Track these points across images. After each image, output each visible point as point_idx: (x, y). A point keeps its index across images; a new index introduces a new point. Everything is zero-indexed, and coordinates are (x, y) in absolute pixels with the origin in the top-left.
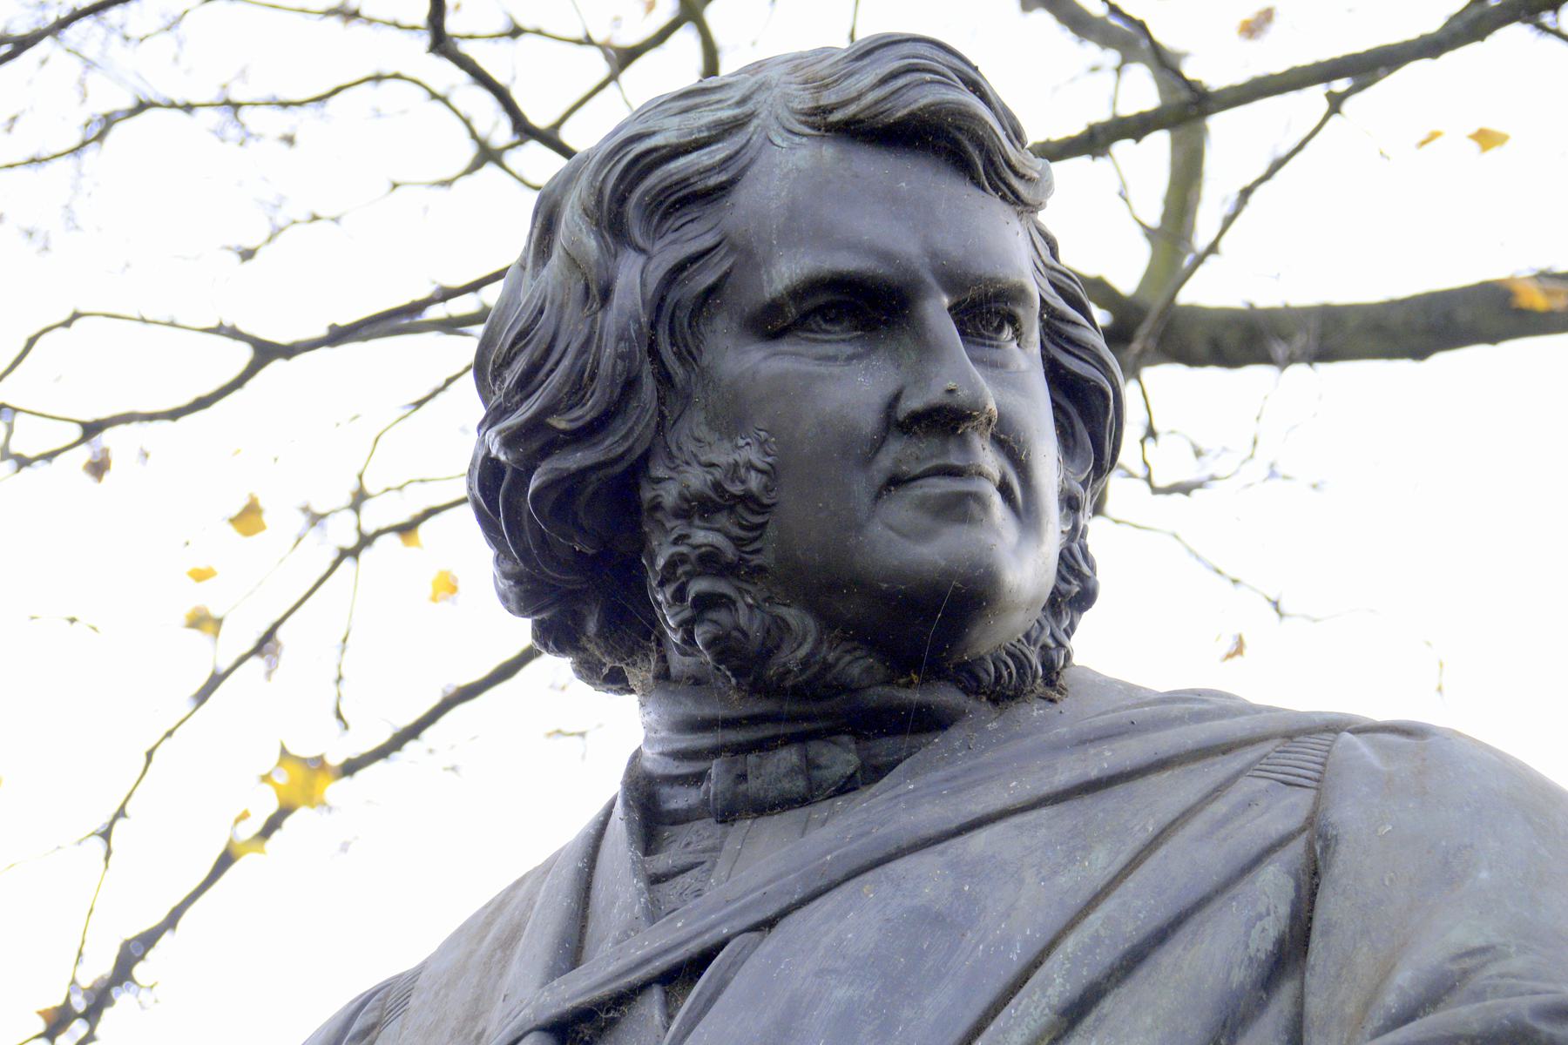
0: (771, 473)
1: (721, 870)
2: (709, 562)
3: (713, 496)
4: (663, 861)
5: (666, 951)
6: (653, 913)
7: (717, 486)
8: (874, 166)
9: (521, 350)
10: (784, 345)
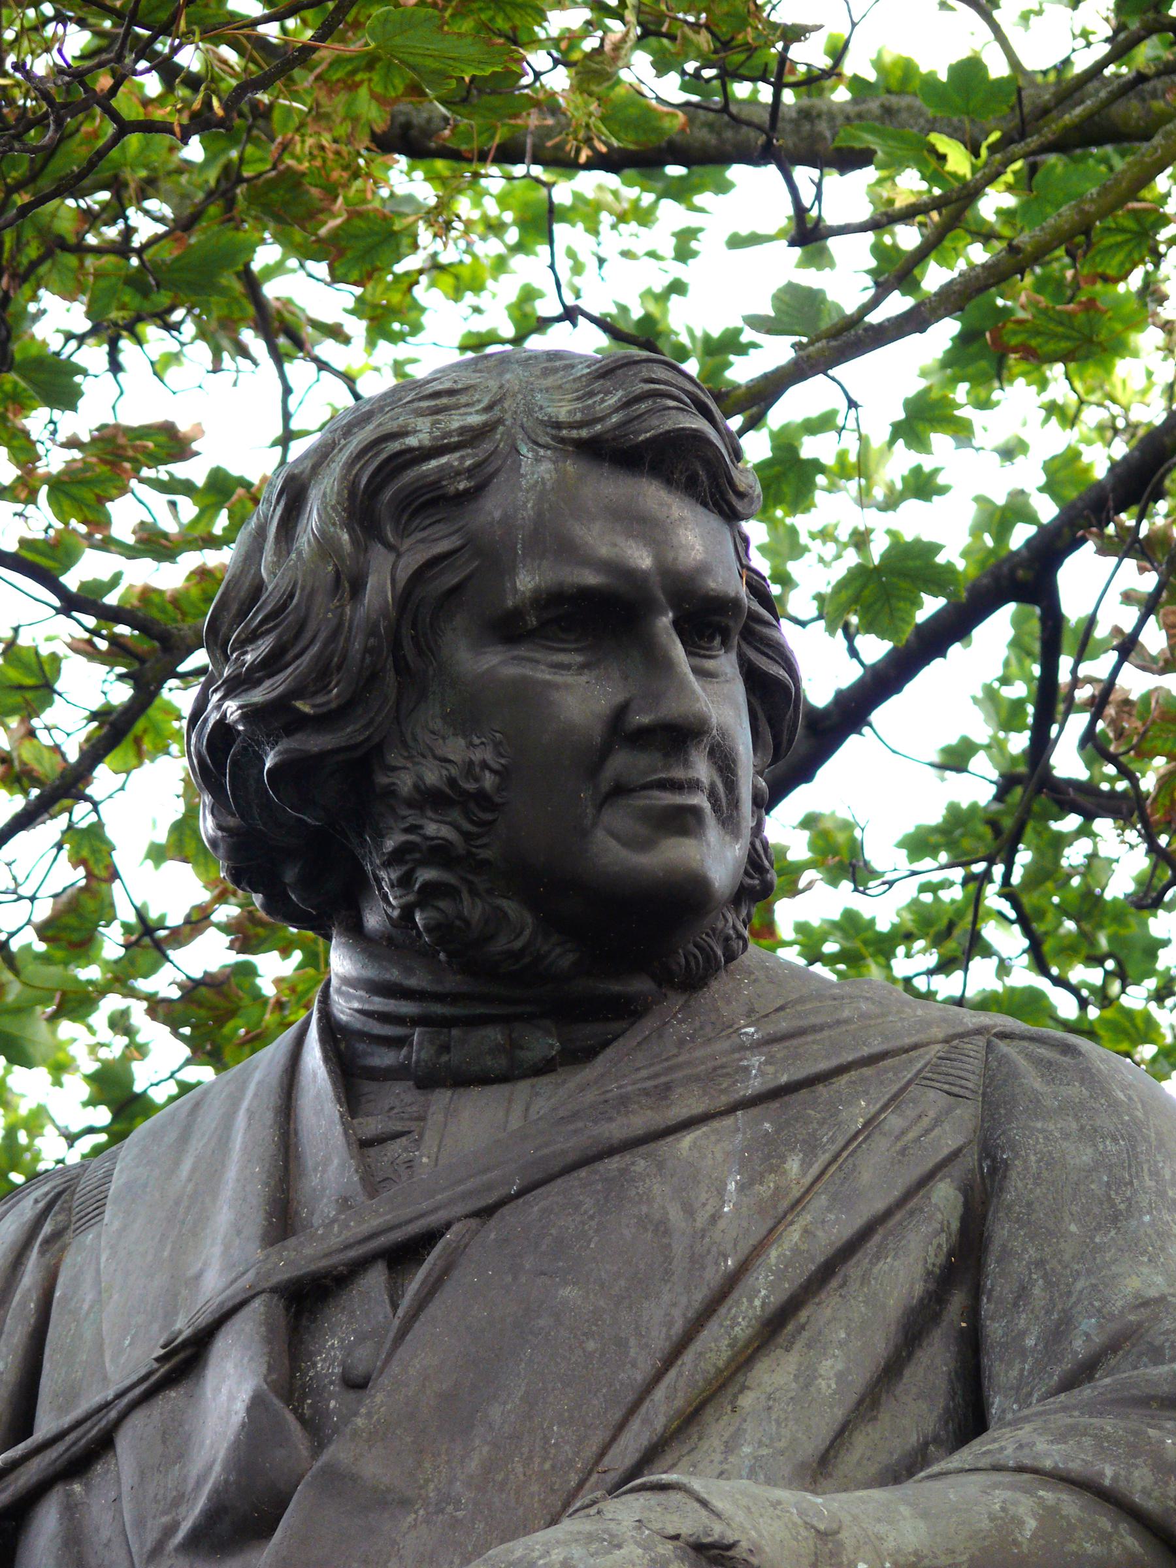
0: (503, 774)
1: (430, 1139)
2: (439, 854)
3: (447, 790)
4: (372, 1126)
5: (391, 1228)
6: (372, 1184)
7: (452, 782)
8: (609, 487)
9: (269, 631)
10: (522, 651)
